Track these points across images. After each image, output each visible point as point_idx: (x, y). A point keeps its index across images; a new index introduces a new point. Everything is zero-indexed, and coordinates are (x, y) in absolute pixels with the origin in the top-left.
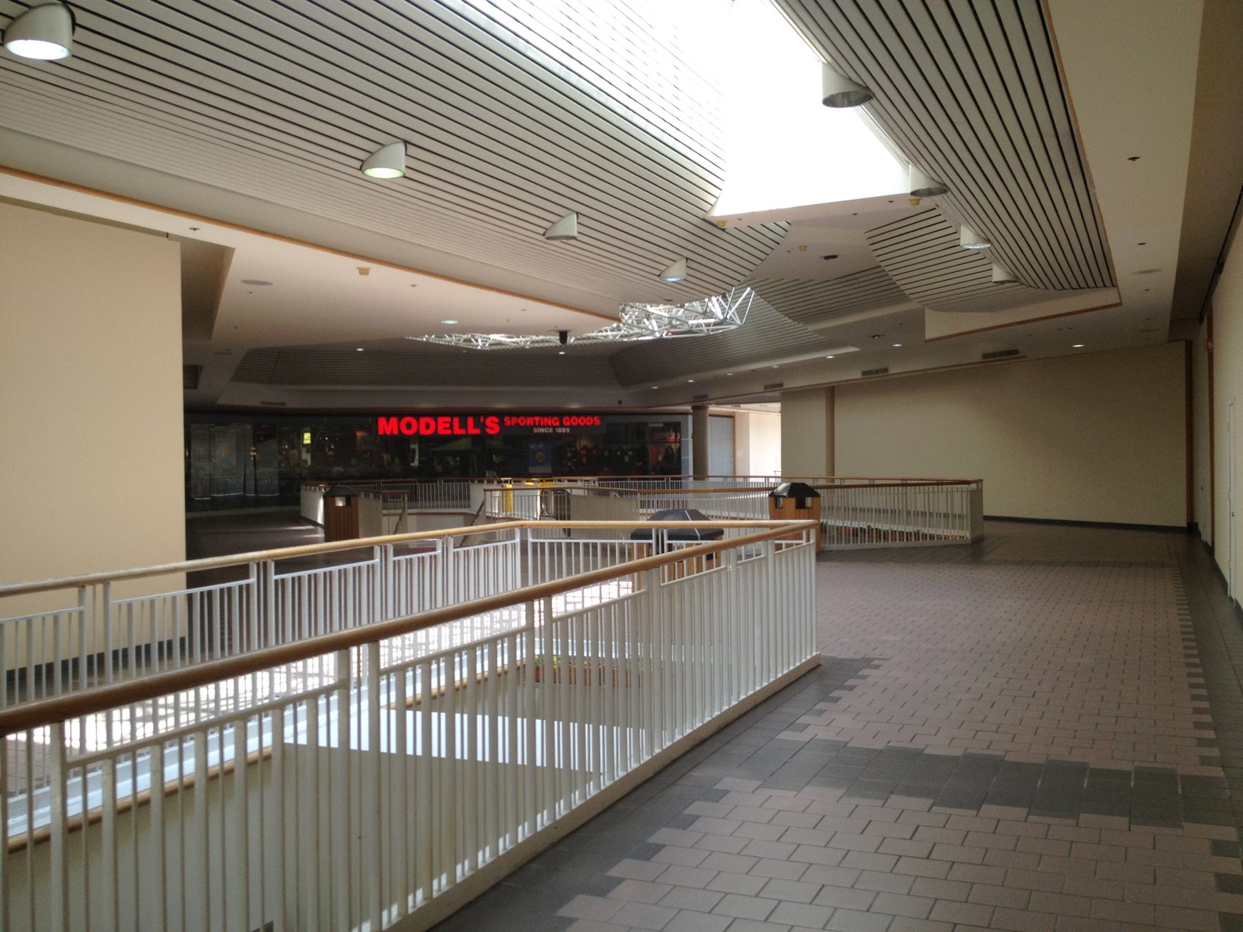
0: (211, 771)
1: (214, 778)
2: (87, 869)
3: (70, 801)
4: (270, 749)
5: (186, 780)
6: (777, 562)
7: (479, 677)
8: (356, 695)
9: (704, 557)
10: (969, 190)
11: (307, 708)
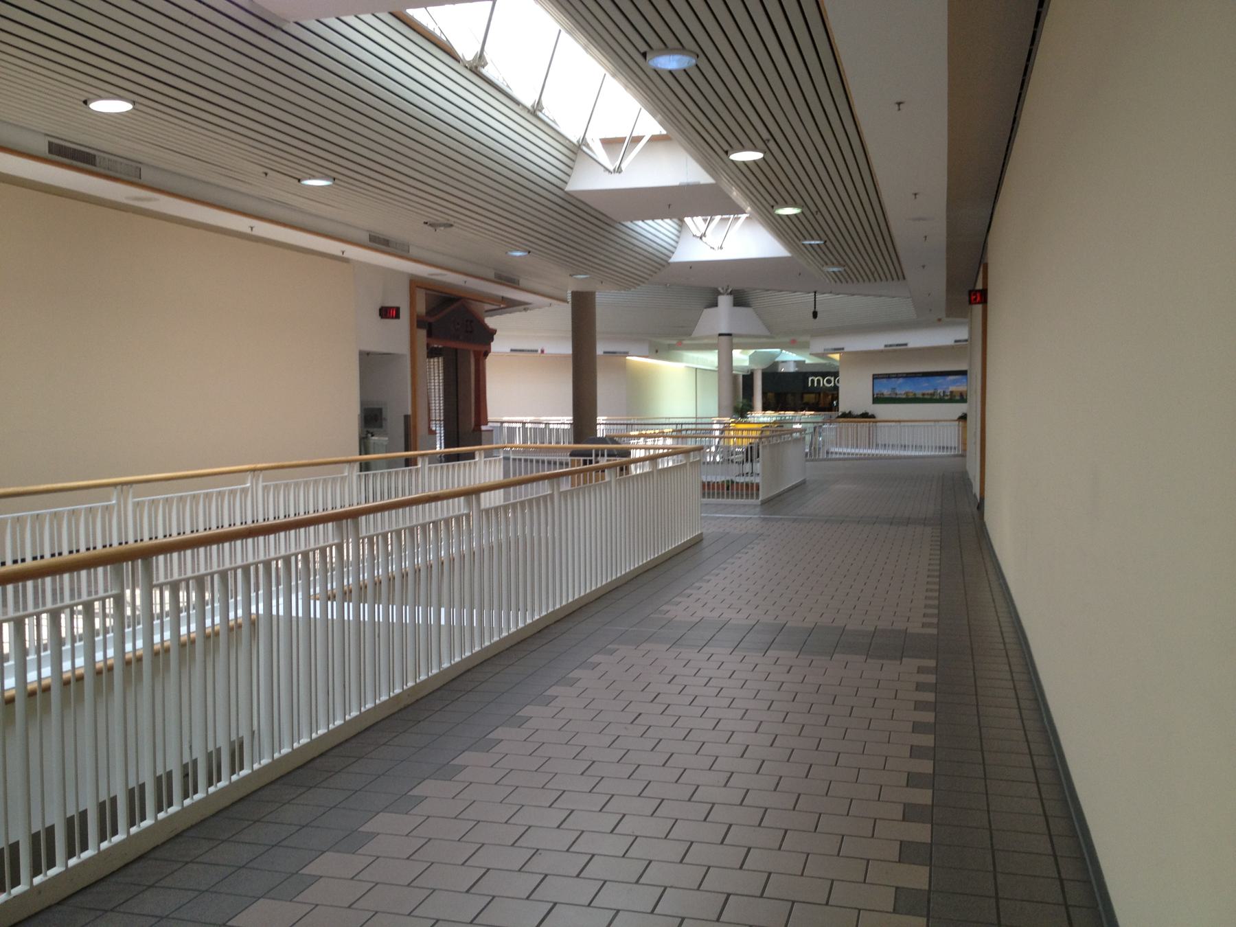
0: (65, 676)
1: (32, 694)
2: (41, 731)
3: (165, 634)
4: (13, 692)
5: (44, 683)
6: (563, 502)
7: (232, 623)
8: (131, 634)
9: (618, 468)
10: (602, 24)
11: (16, 664)
